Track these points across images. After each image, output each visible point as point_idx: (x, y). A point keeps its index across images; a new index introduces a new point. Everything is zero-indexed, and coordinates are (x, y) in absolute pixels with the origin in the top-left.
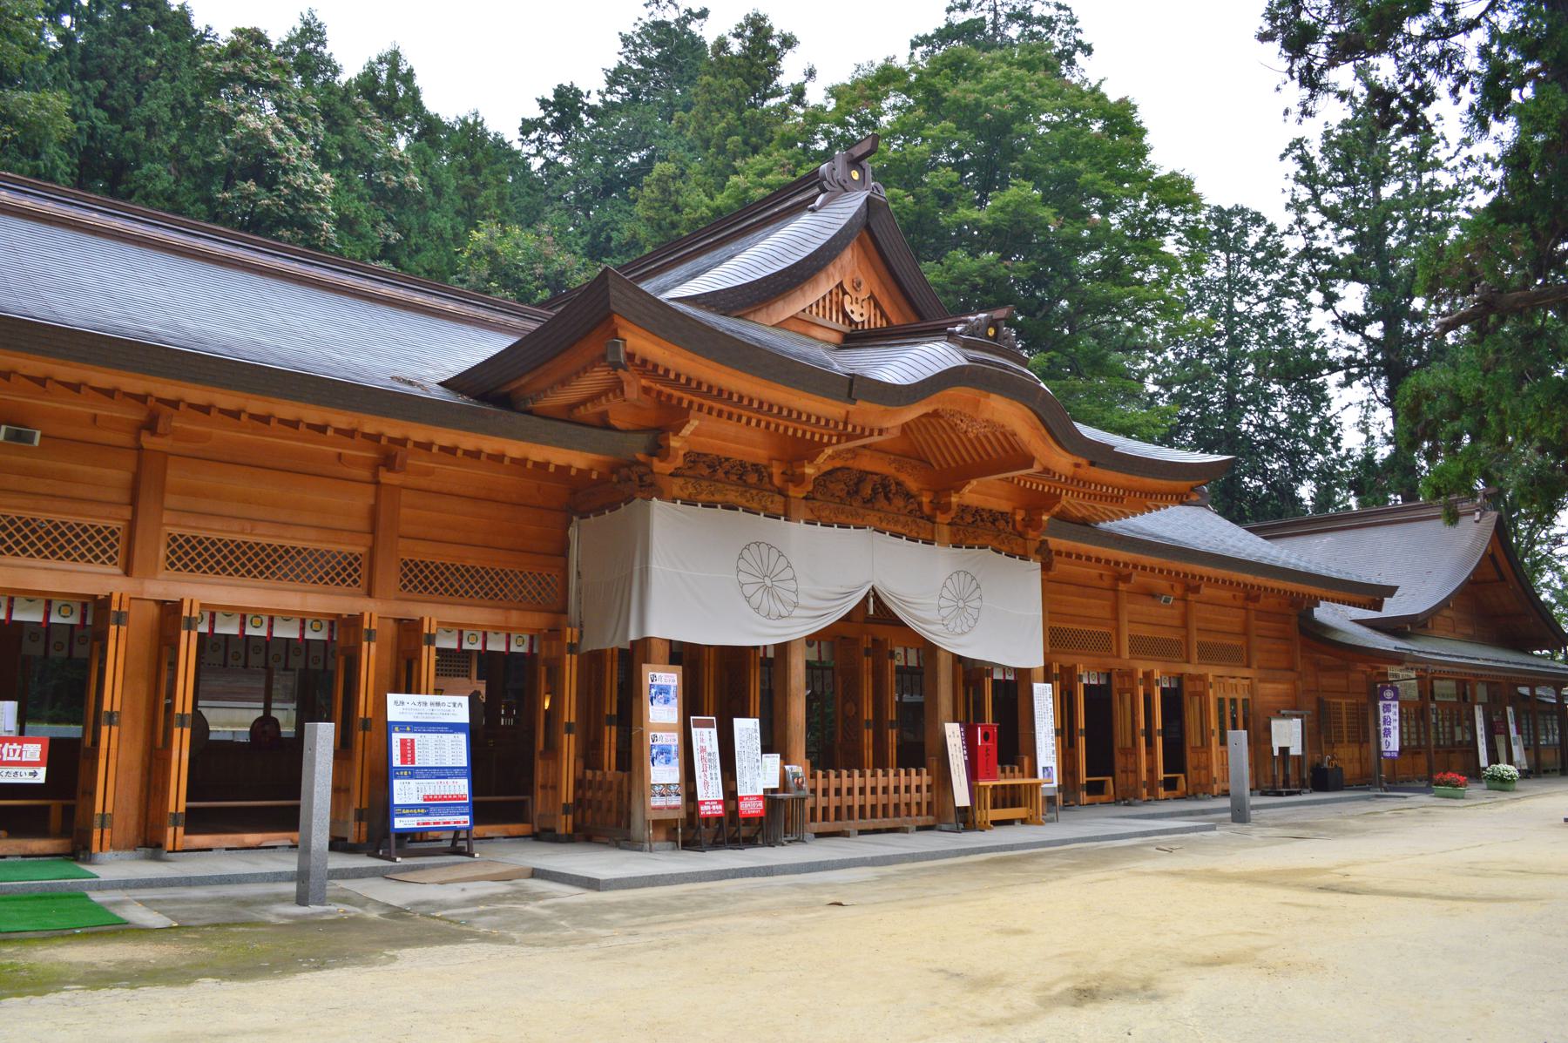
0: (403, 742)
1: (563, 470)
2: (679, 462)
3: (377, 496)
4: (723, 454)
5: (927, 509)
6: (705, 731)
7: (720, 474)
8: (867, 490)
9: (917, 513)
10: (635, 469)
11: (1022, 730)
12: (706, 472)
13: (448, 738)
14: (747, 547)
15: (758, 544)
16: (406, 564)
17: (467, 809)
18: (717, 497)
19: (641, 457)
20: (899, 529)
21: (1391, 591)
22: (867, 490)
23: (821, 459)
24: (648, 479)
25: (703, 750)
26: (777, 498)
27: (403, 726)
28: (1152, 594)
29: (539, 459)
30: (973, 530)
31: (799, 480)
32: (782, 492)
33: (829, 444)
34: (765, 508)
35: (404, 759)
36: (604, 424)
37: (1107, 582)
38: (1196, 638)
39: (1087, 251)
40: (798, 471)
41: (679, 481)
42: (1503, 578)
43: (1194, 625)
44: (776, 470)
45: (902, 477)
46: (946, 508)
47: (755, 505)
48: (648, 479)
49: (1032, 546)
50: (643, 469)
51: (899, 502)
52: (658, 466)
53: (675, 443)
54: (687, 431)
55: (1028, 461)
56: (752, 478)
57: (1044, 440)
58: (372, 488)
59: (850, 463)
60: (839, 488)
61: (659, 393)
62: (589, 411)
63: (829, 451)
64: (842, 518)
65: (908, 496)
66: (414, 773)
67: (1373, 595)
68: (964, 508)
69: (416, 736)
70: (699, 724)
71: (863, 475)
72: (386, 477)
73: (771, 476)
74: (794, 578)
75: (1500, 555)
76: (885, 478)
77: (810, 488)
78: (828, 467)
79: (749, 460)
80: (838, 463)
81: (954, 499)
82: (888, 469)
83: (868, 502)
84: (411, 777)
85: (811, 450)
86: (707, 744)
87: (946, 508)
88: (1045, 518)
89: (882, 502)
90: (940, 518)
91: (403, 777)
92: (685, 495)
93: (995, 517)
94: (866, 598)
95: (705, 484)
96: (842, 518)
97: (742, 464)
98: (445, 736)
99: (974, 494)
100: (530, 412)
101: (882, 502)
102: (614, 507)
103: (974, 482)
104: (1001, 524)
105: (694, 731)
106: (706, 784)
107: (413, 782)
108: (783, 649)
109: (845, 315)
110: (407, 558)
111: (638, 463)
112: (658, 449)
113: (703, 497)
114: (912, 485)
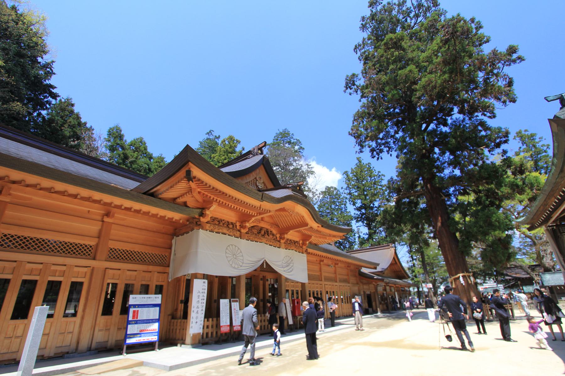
0: (134, 312)
1: (170, 220)
2: (209, 219)
3: (102, 226)
4: (223, 219)
5: (278, 239)
6: (235, 303)
7: (221, 224)
8: (263, 232)
9: (275, 239)
10: (195, 220)
11: (191, 289)
12: (217, 223)
13: (152, 309)
14: (229, 246)
15: (232, 245)
16: (111, 249)
17: (157, 334)
18: (220, 231)
19: (197, 216)
20: (271, 243)
21: (378, 265)
22: (263, 232)
23: (251, 221)
24: (199, 223)
25: (235, 309)
26: (238, 233)
27: (135, 306)
28: (329, 266)
29: (162, 215)
30: (290, 244)
31: (244, 227)
32: (239, 231)
33: (254, 216)
34: (234, 235)
35: (134, 317)
36: (185, 204)
37: (318, 262)
38: (338, 276)
39: (464, 106)
40: (244, 225)
41: (209, 225)
42: (396, 263)
43: (322, 271)
44: (238, 224)
45: (272, 229)
46: (284, 238)
47: (231, 234)
48: (199, 223)
49: (304, 250)
50: (197, 220)
51: (271, 236)
52: (202, 219)
53: (207, 212)
54: (212, 209)
55: (306, 225)
56: (231, 226)
57: (311, 219)
58: (101, 223)
59: (258, 225)
60: (255, 231)
61: (204, 194)
62: (181, 200)
63: (253, 219)
64: (256, 239)
65: (273, 235)
66: (137, 322)
67: (375, 265)
68: (288, 239)
69: (139, 309)
70: (234, 301)
71: (261, 229)
72: (106, 219)
73: (236, 226)
74: (242, 256)
75: (396, 258)
76: (267, 229)
77: (247, 230)
78: (252, 225)
79: (230, 221)
80: (255, 224)
81: (286, 236)
82: (269, 227)
83: (263, 236)
84: (136, 323)
85: (250, 217)
86: (236, 307)
87: (284, 238)
88: (307, 243)
89: (266, 236)
90: (282, 241)
91: (133, 324)
92: (210, 229)
93: (295, 242)
94: (263, 263)
95: (217, 226)
96: (256, 239)
97: (228, 222)
98: (151, 309)
99: (292, 235)
100: (160, 199)
101: (266, 236)
102: (187, 233)
103: (291, 231)
104: (296, 244)
105: (232, 303)
106: (235, 320)
107: (136, 325)
108: (238, 278)
109: (257, 186)
110: (112, 247)
111: (196, 218)
112: (202, 215)
113: (216, 230)
114: (274, 232)
